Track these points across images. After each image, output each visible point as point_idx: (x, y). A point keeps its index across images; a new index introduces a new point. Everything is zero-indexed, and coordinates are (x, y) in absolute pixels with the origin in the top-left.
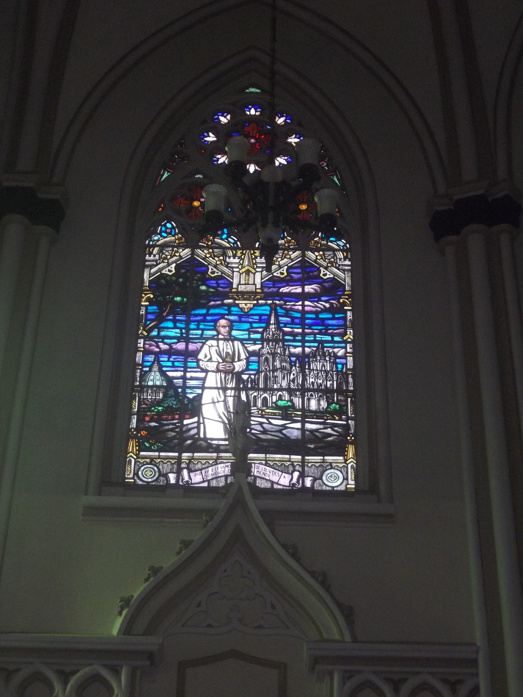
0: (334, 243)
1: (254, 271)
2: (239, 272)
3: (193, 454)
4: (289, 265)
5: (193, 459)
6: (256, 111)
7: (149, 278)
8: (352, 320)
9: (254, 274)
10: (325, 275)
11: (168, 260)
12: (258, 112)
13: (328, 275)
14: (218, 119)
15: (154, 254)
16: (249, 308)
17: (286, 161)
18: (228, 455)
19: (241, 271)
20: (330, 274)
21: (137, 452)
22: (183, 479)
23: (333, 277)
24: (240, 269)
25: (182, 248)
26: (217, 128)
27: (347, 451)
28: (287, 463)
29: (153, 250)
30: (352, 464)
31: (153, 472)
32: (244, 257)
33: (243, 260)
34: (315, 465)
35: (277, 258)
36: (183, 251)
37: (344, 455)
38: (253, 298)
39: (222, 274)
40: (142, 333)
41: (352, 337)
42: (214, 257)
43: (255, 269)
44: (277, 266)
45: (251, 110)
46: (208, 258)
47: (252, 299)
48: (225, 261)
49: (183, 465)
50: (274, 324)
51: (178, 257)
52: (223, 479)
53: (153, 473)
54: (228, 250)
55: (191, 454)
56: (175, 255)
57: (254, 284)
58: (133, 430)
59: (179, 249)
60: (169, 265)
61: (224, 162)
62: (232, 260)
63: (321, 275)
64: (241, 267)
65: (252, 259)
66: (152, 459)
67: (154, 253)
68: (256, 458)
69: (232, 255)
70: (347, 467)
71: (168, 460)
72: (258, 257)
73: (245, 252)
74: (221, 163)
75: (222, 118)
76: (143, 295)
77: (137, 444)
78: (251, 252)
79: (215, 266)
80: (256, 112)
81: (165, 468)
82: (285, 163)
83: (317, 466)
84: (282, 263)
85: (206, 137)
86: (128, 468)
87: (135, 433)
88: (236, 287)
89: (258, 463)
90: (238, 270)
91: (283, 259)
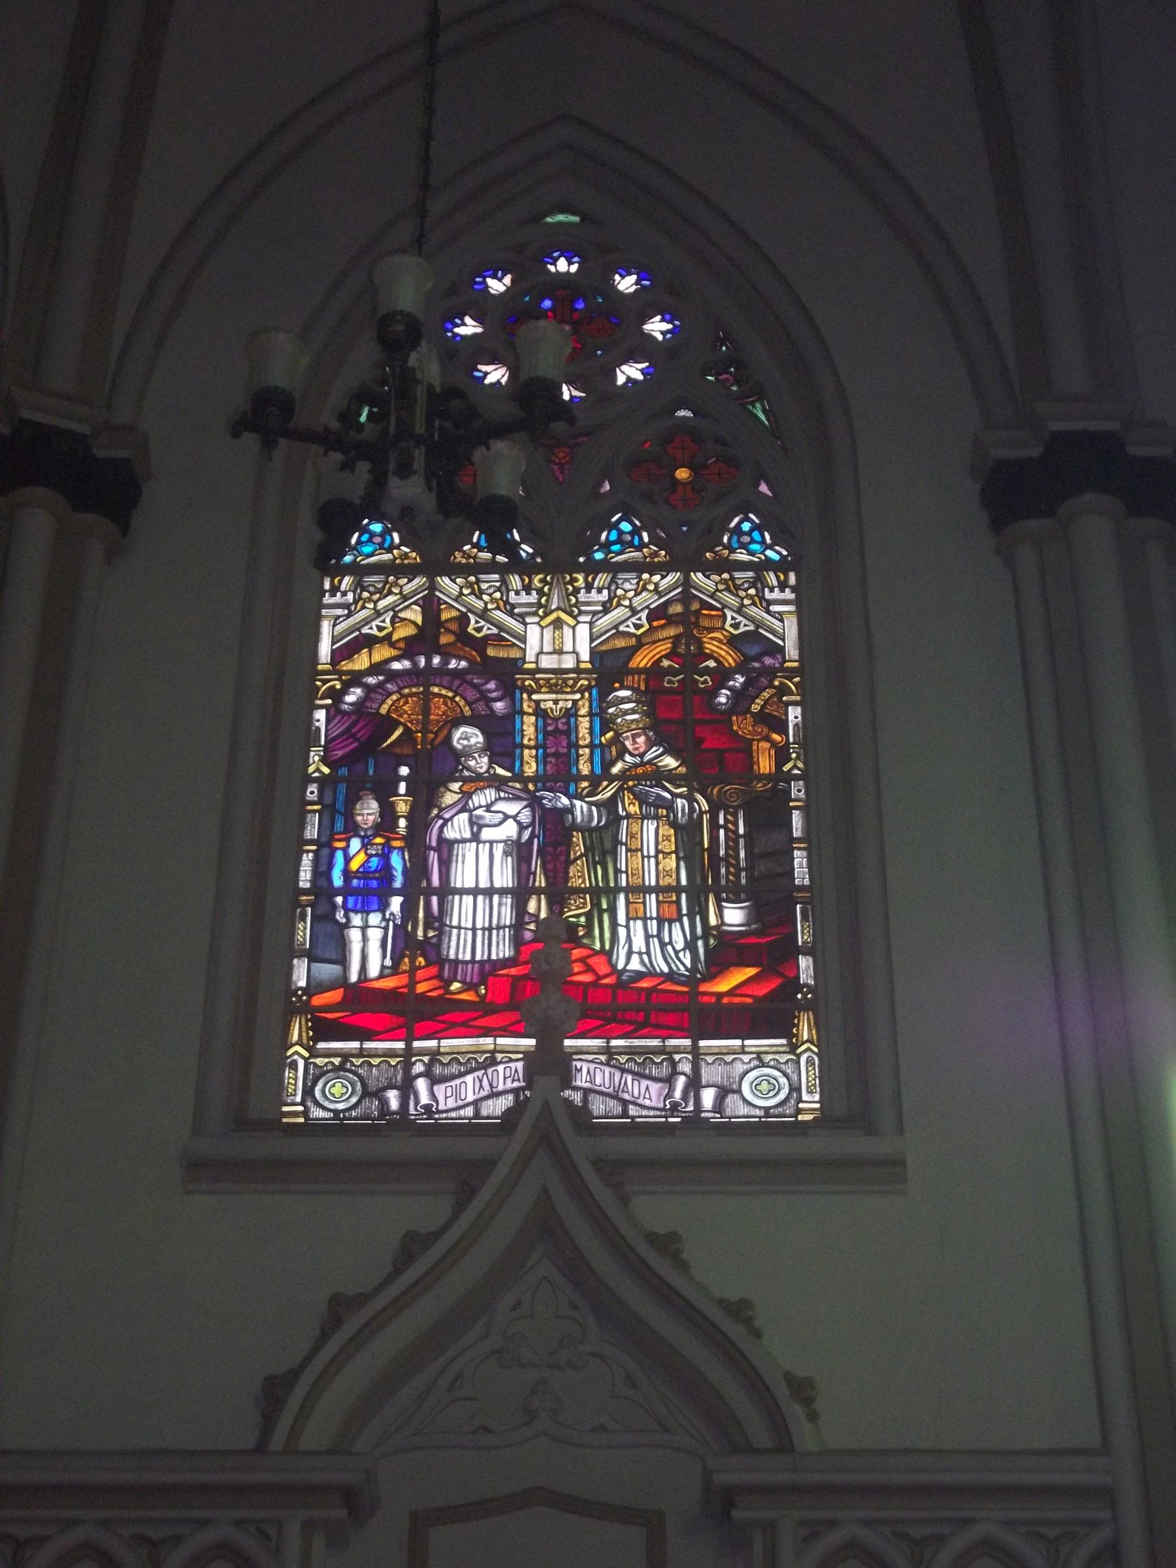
1: (572, 622)
4: (652, 607)
5: (440, 1053)
6: (570, 263)
7: (333, 644)
8: (801, 725)
9: (574, 628)
10: (736, 626)
11: (375, 603)
12: (573, 263)
13: (742, 624)
14: (484, 283)
15: (344, 590)
16: (564, 710)
17: (642, 374)
19: (543, 623)
20: (747, 623)
22: (417, 1102)
23: (497, 632)
24: (542, 618)
25: (660, 572)
26: (481, 307)
27: (797, 1025)
29: (340, 582)
32: (550, 590)
33: (548, 595)
34: (475, 1059)
35: (626, 591)
37: (788, 1035)
38: (572, 687)
39: (500, 632)
40: (318, 770)
41: (800, 765)
42: (737, 590)
43: (575, 618)
44: (627, 609)
45: (558, 263)
46: (720, 591)
47: (569, 690)
48: (762, 598)
49: (419, 1068)
53: (347, 1092)
54: (765, 573)
55: (603, 1042)
56: (390, 593)
58: (300, 992)
59: (400, 578)
61: (498, 382)
62: (776, 595)
63: (470, 630)
64: (544, 612)
66: (346, 1056)
69: (775, 583)
70: (798, 1062)
71: (646, 1056)
72: (581, 589)
74: (492, 384)
75: (491, 282)
76: (318, 683)
78: (565, 578)
79: (739, 611)
80: (569, 265)
82: (640, 377)
83: (393, 1063)
84: (637, 601)
85: (458, 326)
86: (813, 1082)
87: (304, 998)
88: (533, 659)
89: (590, 1059)
90: (536, 619)
91: (640, 593)
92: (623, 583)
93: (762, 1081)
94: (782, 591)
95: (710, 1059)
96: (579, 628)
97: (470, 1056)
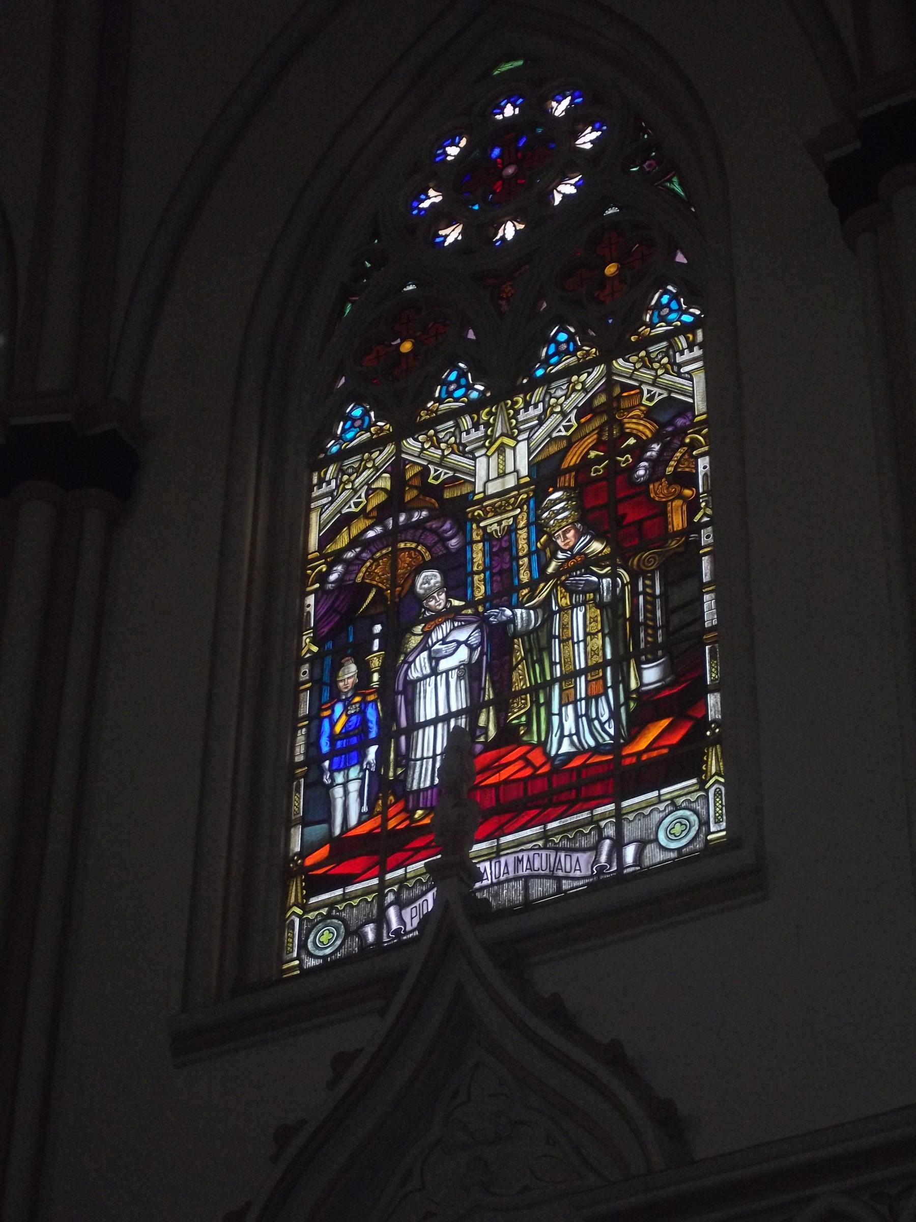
0: (658, 325)
1: (512, 443)
2: (485, 455)
3: (592, 813)
8: (709, 474)
9: (514, 448)
18: (536, 830)
19: (489, 453)
21: (305, 901)
27: (706, 762)
28: (355, 901)
30: (716, 786)
31: (668, 832)
33: (493, 425)
36: (380, 454)
41: (709, 511)
43: (515, 438)
44: (351, 490)
50: (474, 573)
51: (372, 470)
52: (520, 885)
57: (516, 471)
58: (296, 858)
60: (355, 491)
65: (510, 419)
66: (331, 904)
67: (327, 479)
68: (525, 840)
69: (685, 345)
73: (689, 337)
77: (304, 884)
81: (354, 916)
87: (717, 730)
93: (676, 823)
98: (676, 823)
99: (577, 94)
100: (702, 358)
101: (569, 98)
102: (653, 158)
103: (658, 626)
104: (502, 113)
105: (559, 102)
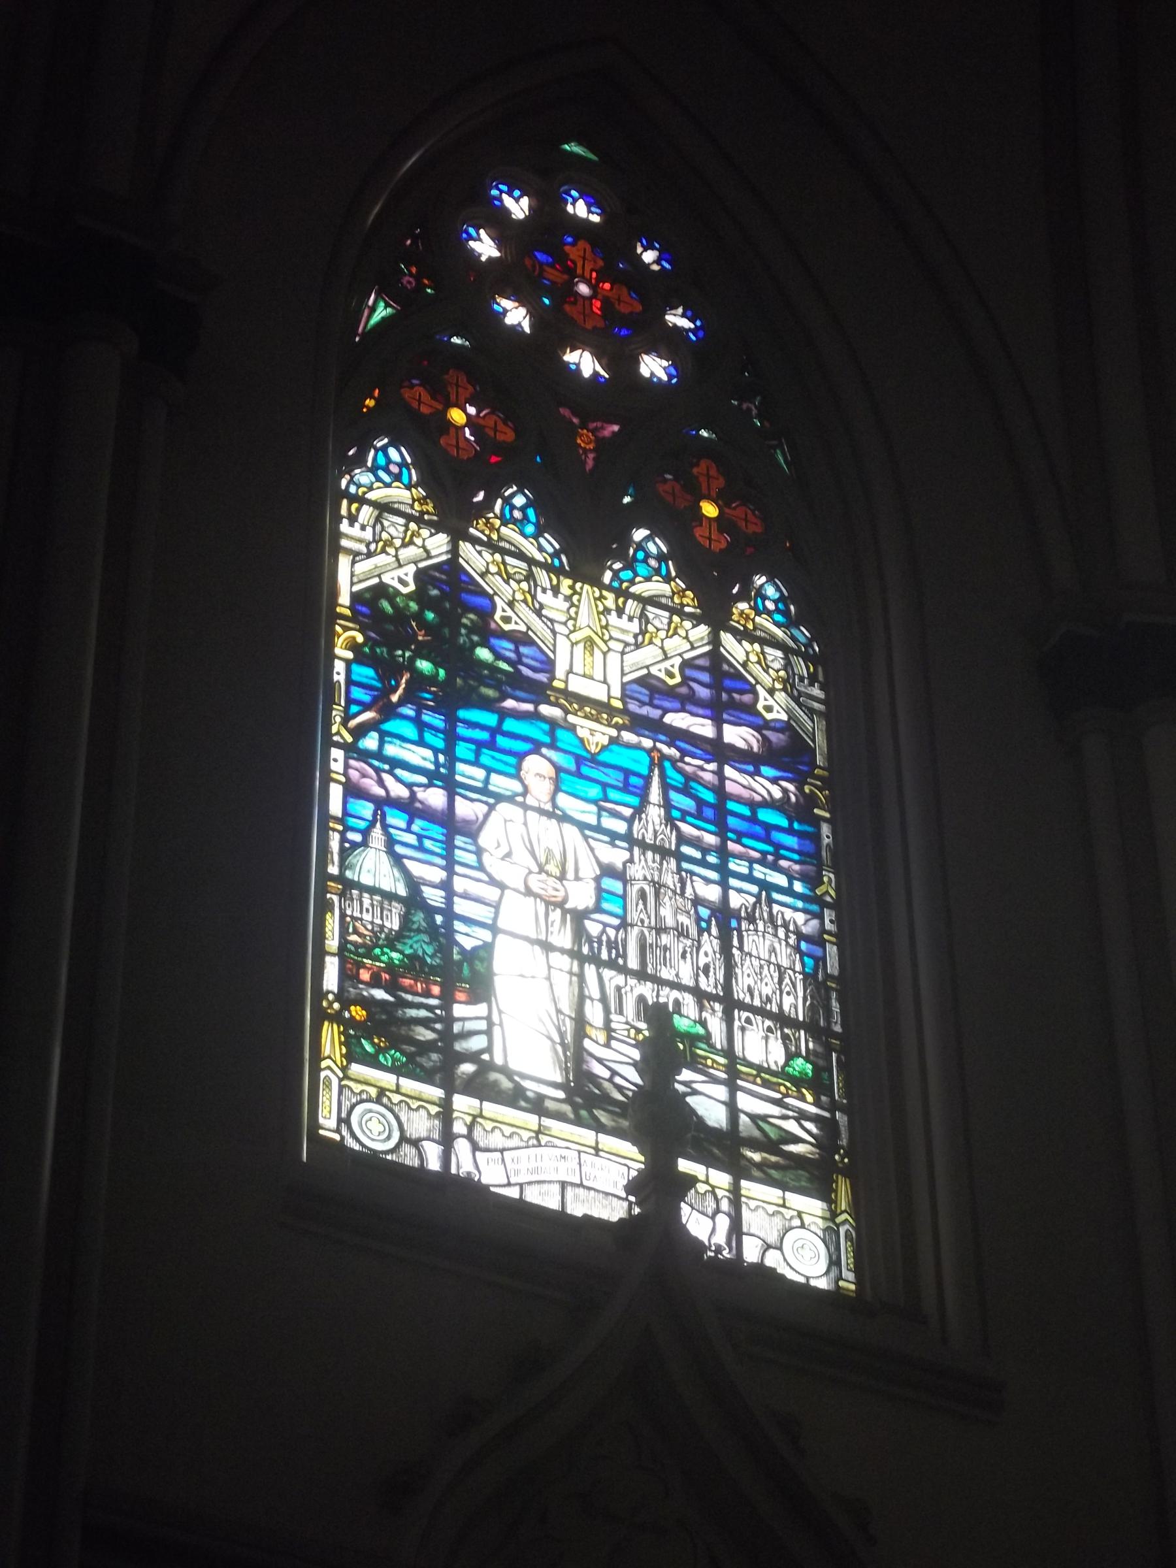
9: (605, 654)
27: (836, 1191)
41: (833, 893)
84: (668, 644)
92: (772, 661)
93: (384, 1127)
94: (811, 684)
95: (753, 1204)
96: (610, 655)
97: (514, 1130)
98: (384, 1127)
99: (701, 334)
100: (415, 597)
101: (692, 326)
102: (420, 288)
103: (443, 906)
104: (645, 250)
105: (683, 315)
